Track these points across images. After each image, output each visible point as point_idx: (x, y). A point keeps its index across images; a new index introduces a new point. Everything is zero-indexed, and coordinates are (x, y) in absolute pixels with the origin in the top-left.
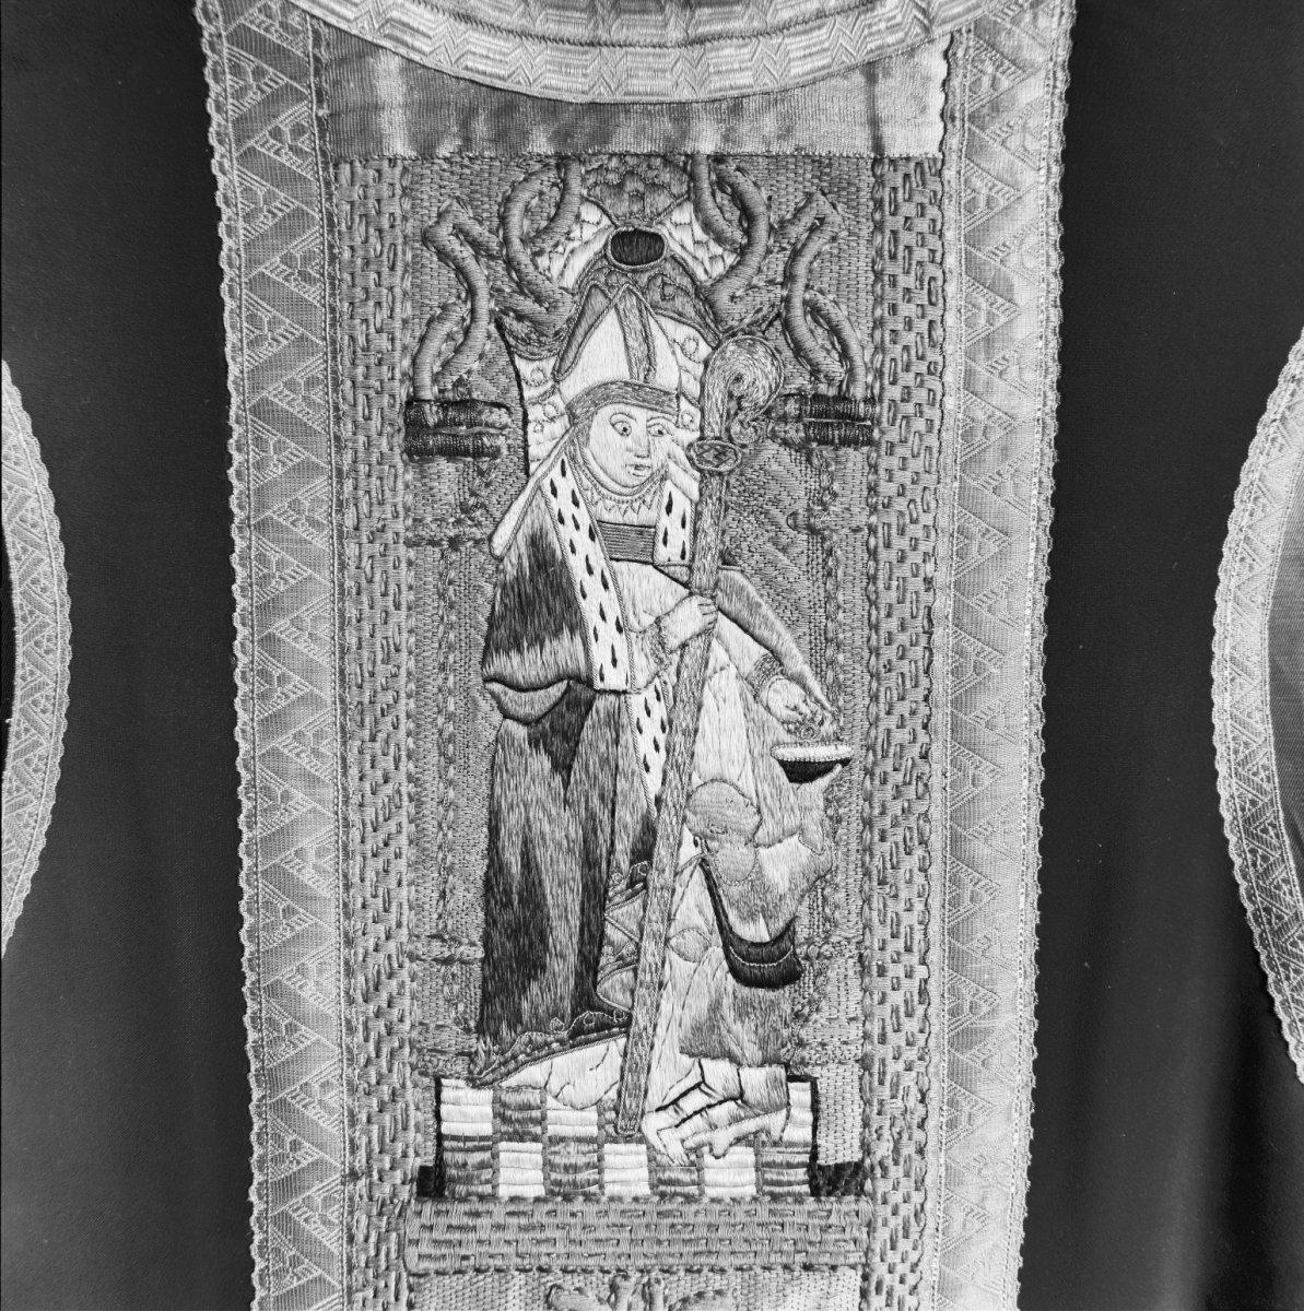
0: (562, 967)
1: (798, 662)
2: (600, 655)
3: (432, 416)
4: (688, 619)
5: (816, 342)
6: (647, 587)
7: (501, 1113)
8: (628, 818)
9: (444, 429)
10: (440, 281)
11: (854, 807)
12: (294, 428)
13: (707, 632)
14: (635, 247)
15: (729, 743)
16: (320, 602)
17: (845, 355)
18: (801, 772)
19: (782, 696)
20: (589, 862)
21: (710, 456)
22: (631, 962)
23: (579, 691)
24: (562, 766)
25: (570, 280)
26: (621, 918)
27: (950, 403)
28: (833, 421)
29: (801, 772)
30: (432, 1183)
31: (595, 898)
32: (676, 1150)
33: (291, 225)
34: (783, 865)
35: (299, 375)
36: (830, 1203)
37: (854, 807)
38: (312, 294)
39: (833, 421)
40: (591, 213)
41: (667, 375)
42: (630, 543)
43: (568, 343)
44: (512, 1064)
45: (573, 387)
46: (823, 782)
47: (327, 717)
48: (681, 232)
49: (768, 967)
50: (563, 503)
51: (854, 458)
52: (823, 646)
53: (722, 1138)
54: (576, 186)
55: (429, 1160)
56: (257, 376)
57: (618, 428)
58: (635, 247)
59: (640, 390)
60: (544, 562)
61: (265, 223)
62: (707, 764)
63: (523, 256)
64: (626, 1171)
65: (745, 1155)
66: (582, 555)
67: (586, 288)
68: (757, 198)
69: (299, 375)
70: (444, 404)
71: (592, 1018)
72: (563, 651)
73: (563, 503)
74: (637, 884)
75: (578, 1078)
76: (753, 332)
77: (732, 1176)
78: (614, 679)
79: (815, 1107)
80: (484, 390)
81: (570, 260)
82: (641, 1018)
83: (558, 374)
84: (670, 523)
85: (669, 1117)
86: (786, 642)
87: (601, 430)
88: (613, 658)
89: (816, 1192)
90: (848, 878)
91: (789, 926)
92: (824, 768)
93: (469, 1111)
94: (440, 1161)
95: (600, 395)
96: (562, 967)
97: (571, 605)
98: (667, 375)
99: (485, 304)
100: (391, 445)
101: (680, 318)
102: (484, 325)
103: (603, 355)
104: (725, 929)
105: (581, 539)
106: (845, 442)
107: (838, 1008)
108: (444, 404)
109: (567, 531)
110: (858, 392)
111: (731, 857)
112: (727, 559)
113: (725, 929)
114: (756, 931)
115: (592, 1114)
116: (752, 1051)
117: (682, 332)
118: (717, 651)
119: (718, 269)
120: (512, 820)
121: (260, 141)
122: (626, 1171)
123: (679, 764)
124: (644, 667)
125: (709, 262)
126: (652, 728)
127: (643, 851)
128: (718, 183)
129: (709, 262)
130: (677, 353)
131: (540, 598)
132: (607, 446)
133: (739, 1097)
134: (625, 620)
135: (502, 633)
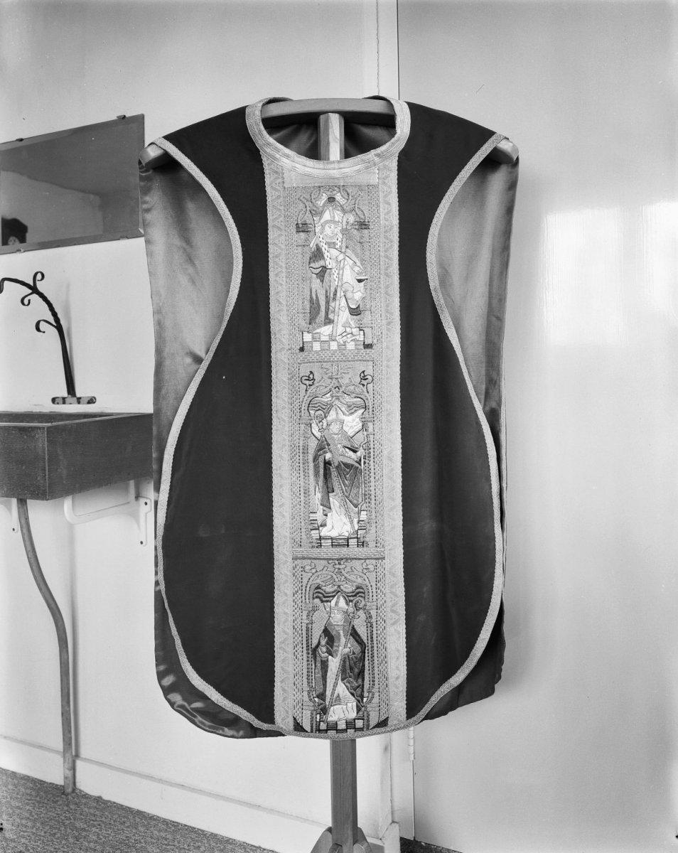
0: (323, 313)
1: (358, 264)
2: (327, 263)
3: (301, 226)
4: (341, 257)
5: (359, 213)
6: (334, 252)
7: (313, 338)
8: (333, 289)
9: (303, 228)
10: (301, 206)
11: (368, 287)
12: (279, 228)
13: (344, 259)
14: (331, 200)
15: (349, 276)
16: (283, 257)
17: (364, 215)
18: (360, 281)
19: (357, 269)
20: (327, 297)
21: (345, 232)
22: (334, 312)
23: (324, 269)
24: (322, 281)
25: (321, 205)
26: (332, 304)
27: (382, 222)
28: (363, 225)
29: (360, 281)
30: (302, 349)
31: (327, 303)
32: (342, 342)
33: (279, 197)
34: (358, 296)
35: (277, 182)
36: (366, 350)
37: (368, 287)
38: (282, 208)
39: (363, 225)
40: (324, 195)
41: (337, 219)
42: (332, 245)
43: (321, 214)
44: (315, 329)
45: (322, 221)
46: (363, 283)
47: (284, 275)
48: (338, 197)
49: (355, 312)
50: (321, 239)
51: (366, 231)
52: (362, 261)
53: (349, 340)
54: (322, 190)
55: (301, 346)
56: (273, 220)
57: (330, 226)
58: (331, 200)
59: (333, 221)
60: (319, 249)
61: (274, 197)
62: (345, 280)
63: (313, 201)
64: (334, 346)
65: (353, 343)
66: (324, 247)
67: (324, 206)
68: (349, 191)
69: (277, 182)
70: (302, 224)
71: (328, 321)
72: (322, 263)
73: (321, 239)
74: (334, 299)
75: (325, 331)
76: (351, 211)
77: (351, 346)
78: (329, 267)
79: (364, 335)
80: (308, 222)
81: (321, 203)
82: (336, 321)
83: (320, 220)
84: (338, 242)
85: (340, 337)
86: (357, 261)
87: (327, 227)
88: (330, 263)
89: (365, 348)
90: (368, 298)
91: (359, 306)
92: (363, 280)
93: (308, 337)
94: (303, 346)
95: (327, 222)
96: (323, 313)
97: (323, 256)
98: (337, 219)
99: (308, 209)
100: (294, 230)
101: (338, 210)
102: (308, 212)
103: (327, 216)
104: (349, 306)
105: (324, 245)
106: (365, 228)
107: (367, 318)
108: (302, 224)
109: (322, 244)
110: (366, 221)
111: (349, 295)
112: (347, 247)
113: (349, 306)
114: (354, 307)
115: (328, 337)
116: (354, 326)
117: (339, 212)
118: (346, 263)
119: (344, 203)
120: (314, 291)
121: (274, 185)
122: (334, 346)
123: (340, 279)
124: (334, 265)
125: (342, 201)
126: (336, 274)
127: (335, 294)
128: (342, 188)
129: (342, 201)
130: (338, 215)
131: (318, 254)
132: (328, 231)
133: (352, 333)
134: (331, 256)
135: (312, 260)
